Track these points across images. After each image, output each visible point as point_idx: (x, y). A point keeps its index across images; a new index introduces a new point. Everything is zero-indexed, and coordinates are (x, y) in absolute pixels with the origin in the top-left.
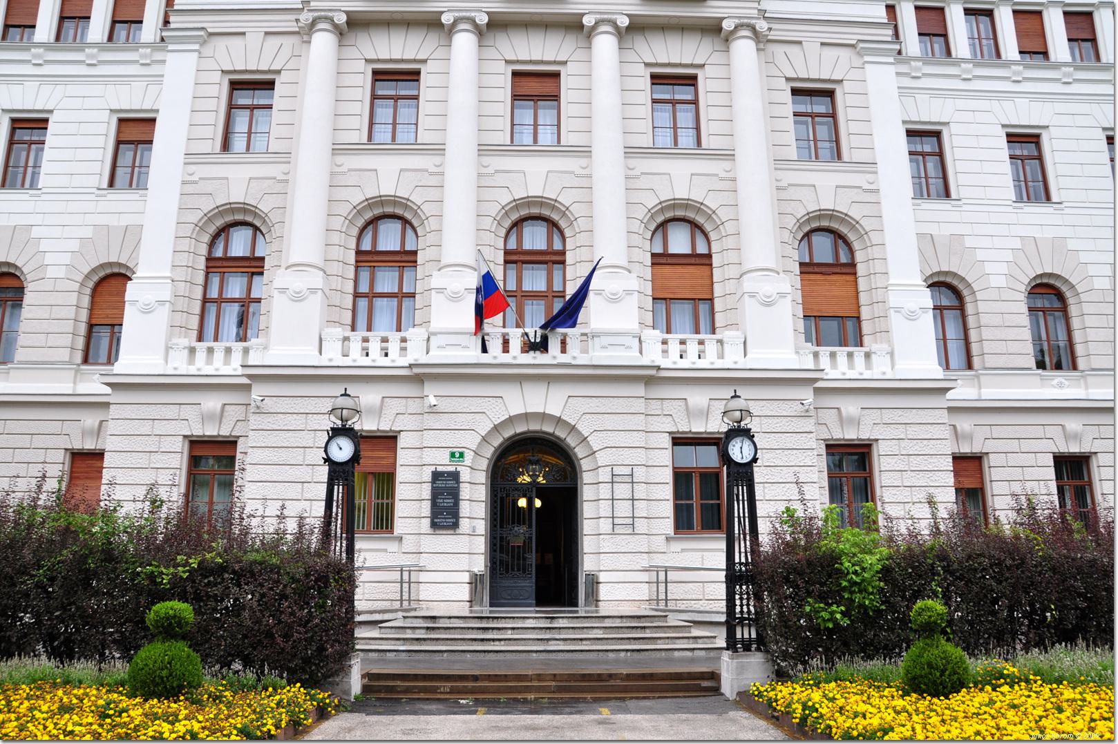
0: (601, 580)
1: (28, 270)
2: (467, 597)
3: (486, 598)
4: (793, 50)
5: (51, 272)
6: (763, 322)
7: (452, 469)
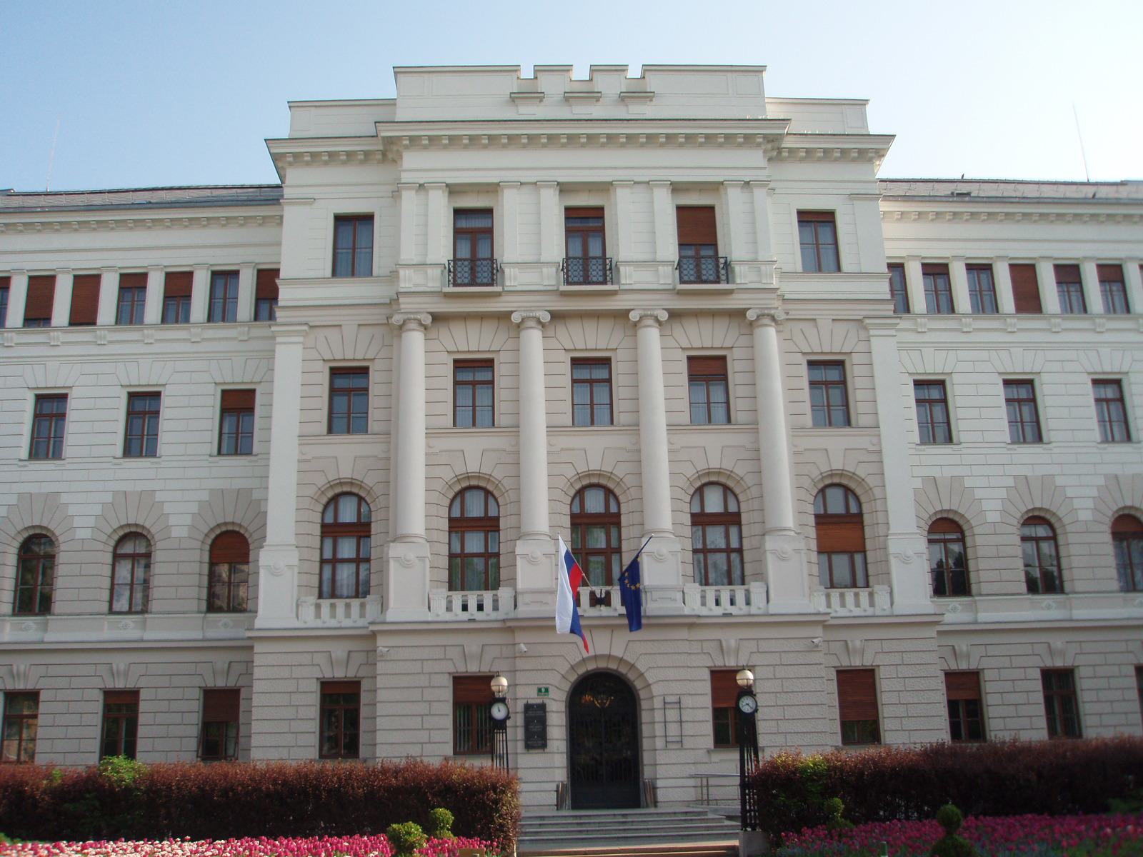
0: (658, 786)
1: (155, 530)
2: (555, 802)
3: (568, 802)
4: (807, 327)
5: (175, 533)
6: (788, 570)
7: (539, 701)
